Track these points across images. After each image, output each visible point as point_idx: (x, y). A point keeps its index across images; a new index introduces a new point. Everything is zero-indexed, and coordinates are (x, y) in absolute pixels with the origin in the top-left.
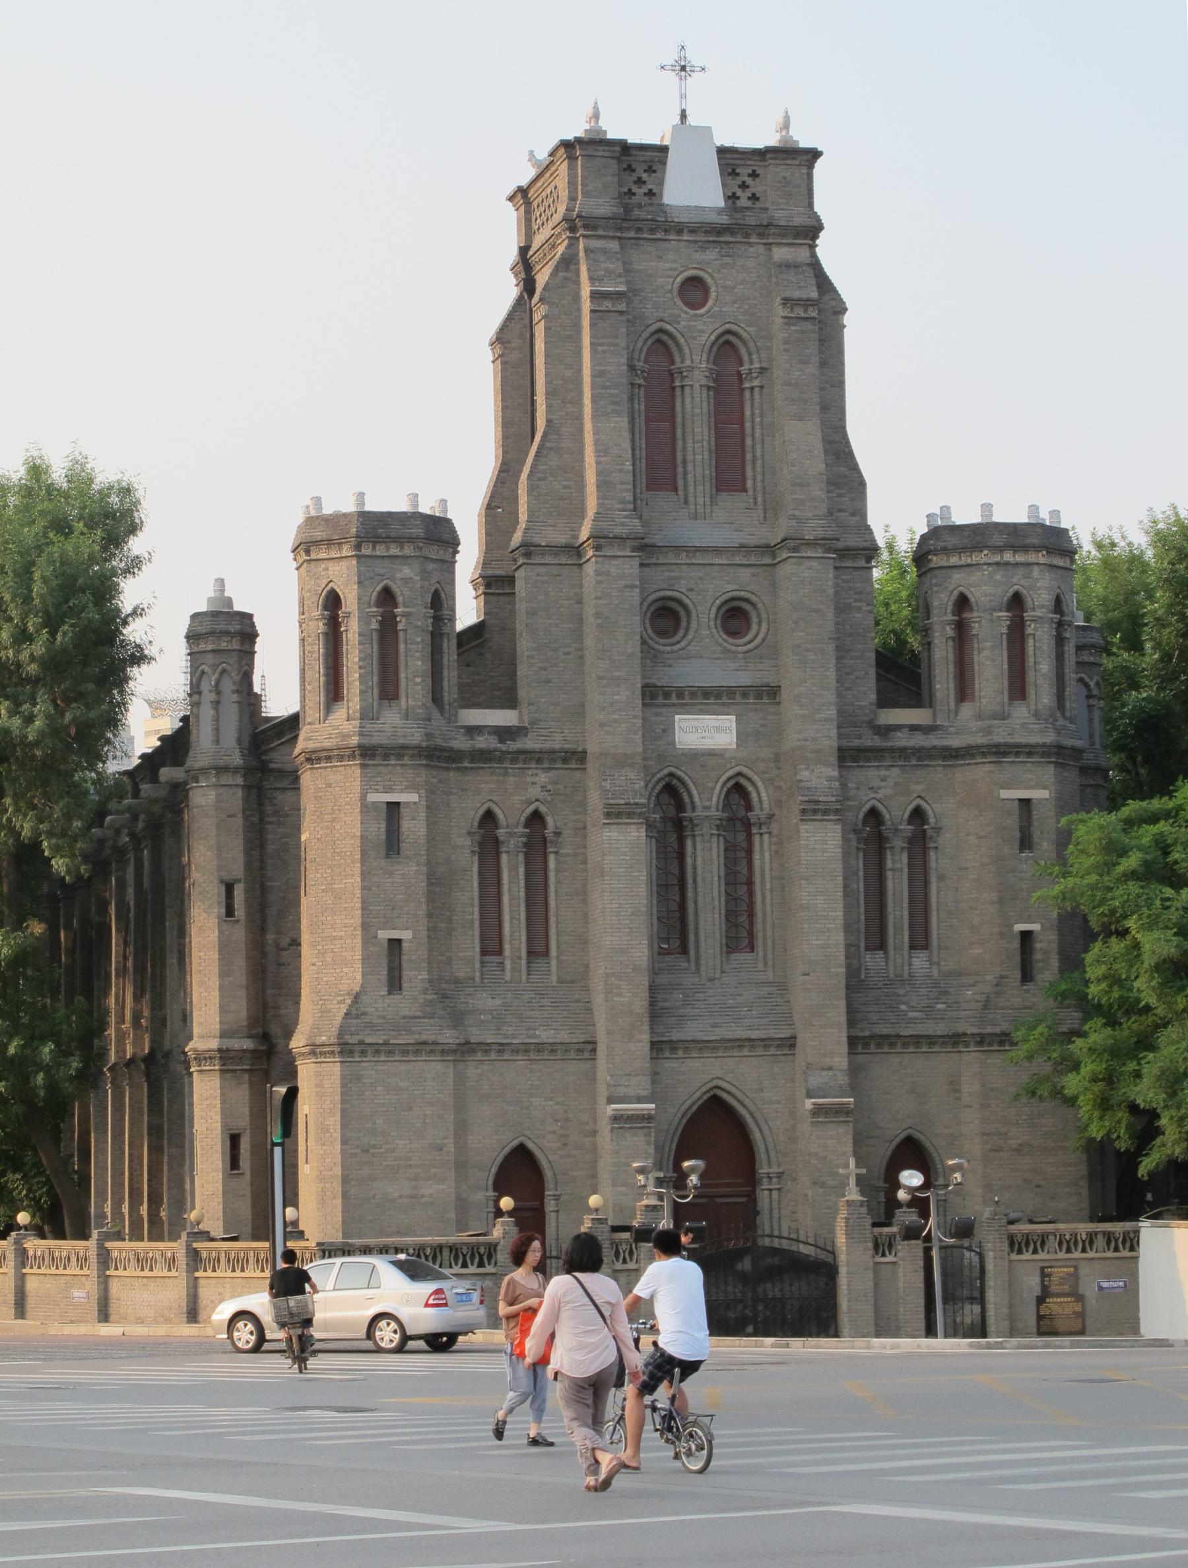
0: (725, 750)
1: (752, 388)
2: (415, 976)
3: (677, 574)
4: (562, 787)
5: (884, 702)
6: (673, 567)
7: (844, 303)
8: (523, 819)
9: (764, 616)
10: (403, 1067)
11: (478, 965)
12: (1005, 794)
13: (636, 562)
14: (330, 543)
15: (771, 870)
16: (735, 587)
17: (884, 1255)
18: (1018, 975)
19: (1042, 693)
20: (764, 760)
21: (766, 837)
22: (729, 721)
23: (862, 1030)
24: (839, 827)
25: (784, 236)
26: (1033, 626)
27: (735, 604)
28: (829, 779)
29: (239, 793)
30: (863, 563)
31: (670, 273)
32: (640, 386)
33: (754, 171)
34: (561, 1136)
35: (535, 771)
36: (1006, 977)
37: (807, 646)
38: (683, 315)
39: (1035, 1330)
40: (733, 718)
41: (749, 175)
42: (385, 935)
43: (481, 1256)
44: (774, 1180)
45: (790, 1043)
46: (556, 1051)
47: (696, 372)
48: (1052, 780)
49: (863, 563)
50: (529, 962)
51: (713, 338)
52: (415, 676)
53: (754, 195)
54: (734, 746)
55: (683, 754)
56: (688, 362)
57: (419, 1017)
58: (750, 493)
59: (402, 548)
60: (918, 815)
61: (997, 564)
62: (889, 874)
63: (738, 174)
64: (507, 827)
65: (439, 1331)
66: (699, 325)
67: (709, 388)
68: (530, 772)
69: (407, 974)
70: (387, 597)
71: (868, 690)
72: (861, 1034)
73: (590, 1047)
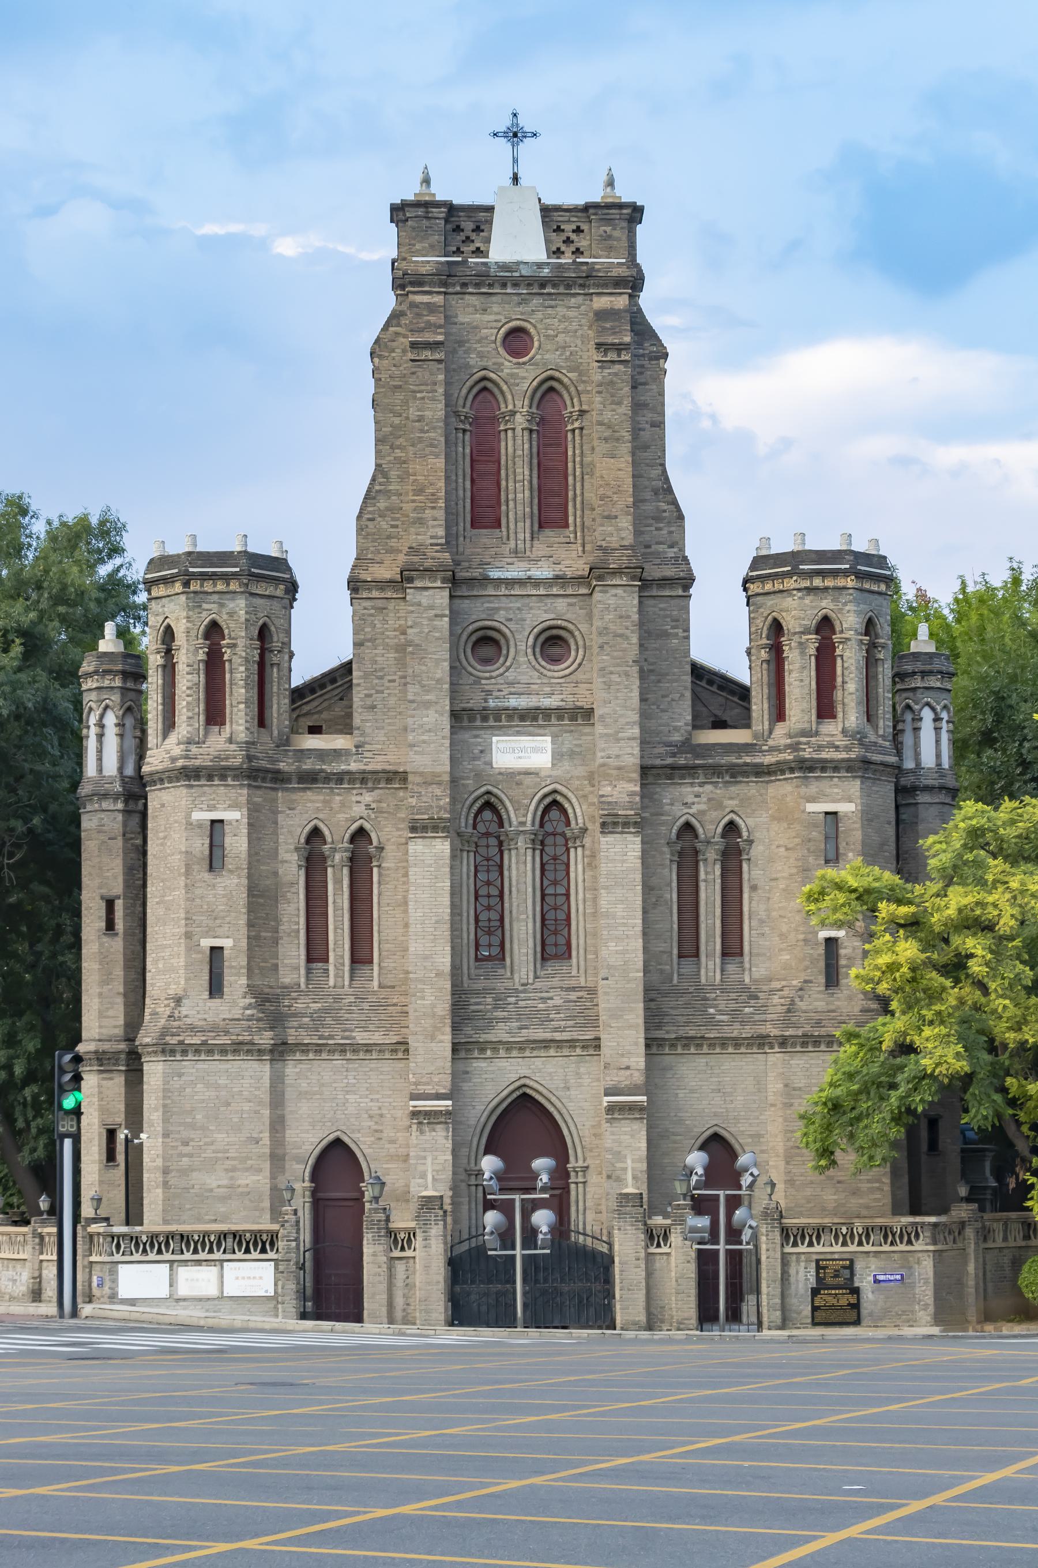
0: (540, 769)
1: (573, 430)
2: (236, 982)
3: (497, 605)
4: (385, 805)
5: (697, 724)
6: (492, 598)
7: (665, 348)
8: (347, 836)
9: (581, 643)
10: (224, 1066)
11: (303, 971)
12: (811, 807)
13: (446, 593)
14: (165, 581)
15: (584, 880)
16: (552, 616)
17: (659, 1246)
18: (822, 980)
19: (850, 715)
20: (578, 778)
21: (579, 850)
22: (545, 742)
23: (668, 1032)
24: (639, 839)
25: (605, 286)
26: (841, 647)
27: (555, 632)
28: (632, 794)
29: (120, 817)
30: (680, 592)
31: (495, 324)
32: (464, 431)
33: (578, 227)
34: (376, 1131)
35: (360, 791)
36: (810, 982)
37: (612, 669)
38: (507, 363)
39: (809, 1320)
40: (549, 739)
41: (574, 231)
42: (207, 943)
43: (264, 1243)
44: (580, 1174)
45: (596, 1044)
46: (371, 1051)
47: (518, 416)
48: (858, 794)
49: (680, 592)
50: (352, 971)
51: (535, 383)
52: (239, 703)
53: (578, 249)
54: (550, 765)
55: (500, 774)
56: (510, 407)
57: (238, 1020)
58: (571, 528)
59: (228, 585)
60: (731, 828)
61: (806, 588)
62: (702, 886)
63: (563, 231)
64: (333, 842)
65: (861, 1296)
66: (521, 372)
67: (531, 431)
68: (355, 792)
69: (228, 979)
70: (214, 630)
71: (683, 713)
72: (666, 1036)
73: (403, 1048)
